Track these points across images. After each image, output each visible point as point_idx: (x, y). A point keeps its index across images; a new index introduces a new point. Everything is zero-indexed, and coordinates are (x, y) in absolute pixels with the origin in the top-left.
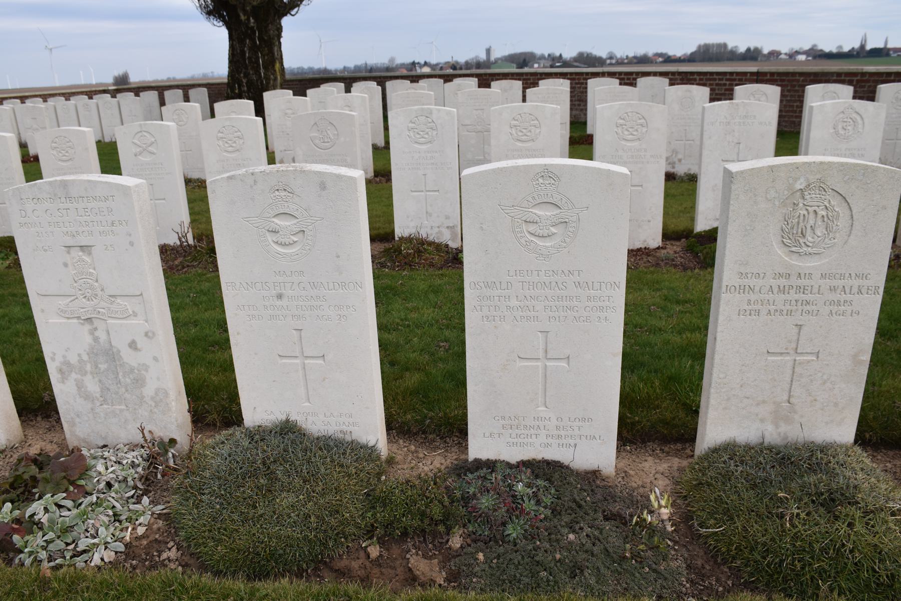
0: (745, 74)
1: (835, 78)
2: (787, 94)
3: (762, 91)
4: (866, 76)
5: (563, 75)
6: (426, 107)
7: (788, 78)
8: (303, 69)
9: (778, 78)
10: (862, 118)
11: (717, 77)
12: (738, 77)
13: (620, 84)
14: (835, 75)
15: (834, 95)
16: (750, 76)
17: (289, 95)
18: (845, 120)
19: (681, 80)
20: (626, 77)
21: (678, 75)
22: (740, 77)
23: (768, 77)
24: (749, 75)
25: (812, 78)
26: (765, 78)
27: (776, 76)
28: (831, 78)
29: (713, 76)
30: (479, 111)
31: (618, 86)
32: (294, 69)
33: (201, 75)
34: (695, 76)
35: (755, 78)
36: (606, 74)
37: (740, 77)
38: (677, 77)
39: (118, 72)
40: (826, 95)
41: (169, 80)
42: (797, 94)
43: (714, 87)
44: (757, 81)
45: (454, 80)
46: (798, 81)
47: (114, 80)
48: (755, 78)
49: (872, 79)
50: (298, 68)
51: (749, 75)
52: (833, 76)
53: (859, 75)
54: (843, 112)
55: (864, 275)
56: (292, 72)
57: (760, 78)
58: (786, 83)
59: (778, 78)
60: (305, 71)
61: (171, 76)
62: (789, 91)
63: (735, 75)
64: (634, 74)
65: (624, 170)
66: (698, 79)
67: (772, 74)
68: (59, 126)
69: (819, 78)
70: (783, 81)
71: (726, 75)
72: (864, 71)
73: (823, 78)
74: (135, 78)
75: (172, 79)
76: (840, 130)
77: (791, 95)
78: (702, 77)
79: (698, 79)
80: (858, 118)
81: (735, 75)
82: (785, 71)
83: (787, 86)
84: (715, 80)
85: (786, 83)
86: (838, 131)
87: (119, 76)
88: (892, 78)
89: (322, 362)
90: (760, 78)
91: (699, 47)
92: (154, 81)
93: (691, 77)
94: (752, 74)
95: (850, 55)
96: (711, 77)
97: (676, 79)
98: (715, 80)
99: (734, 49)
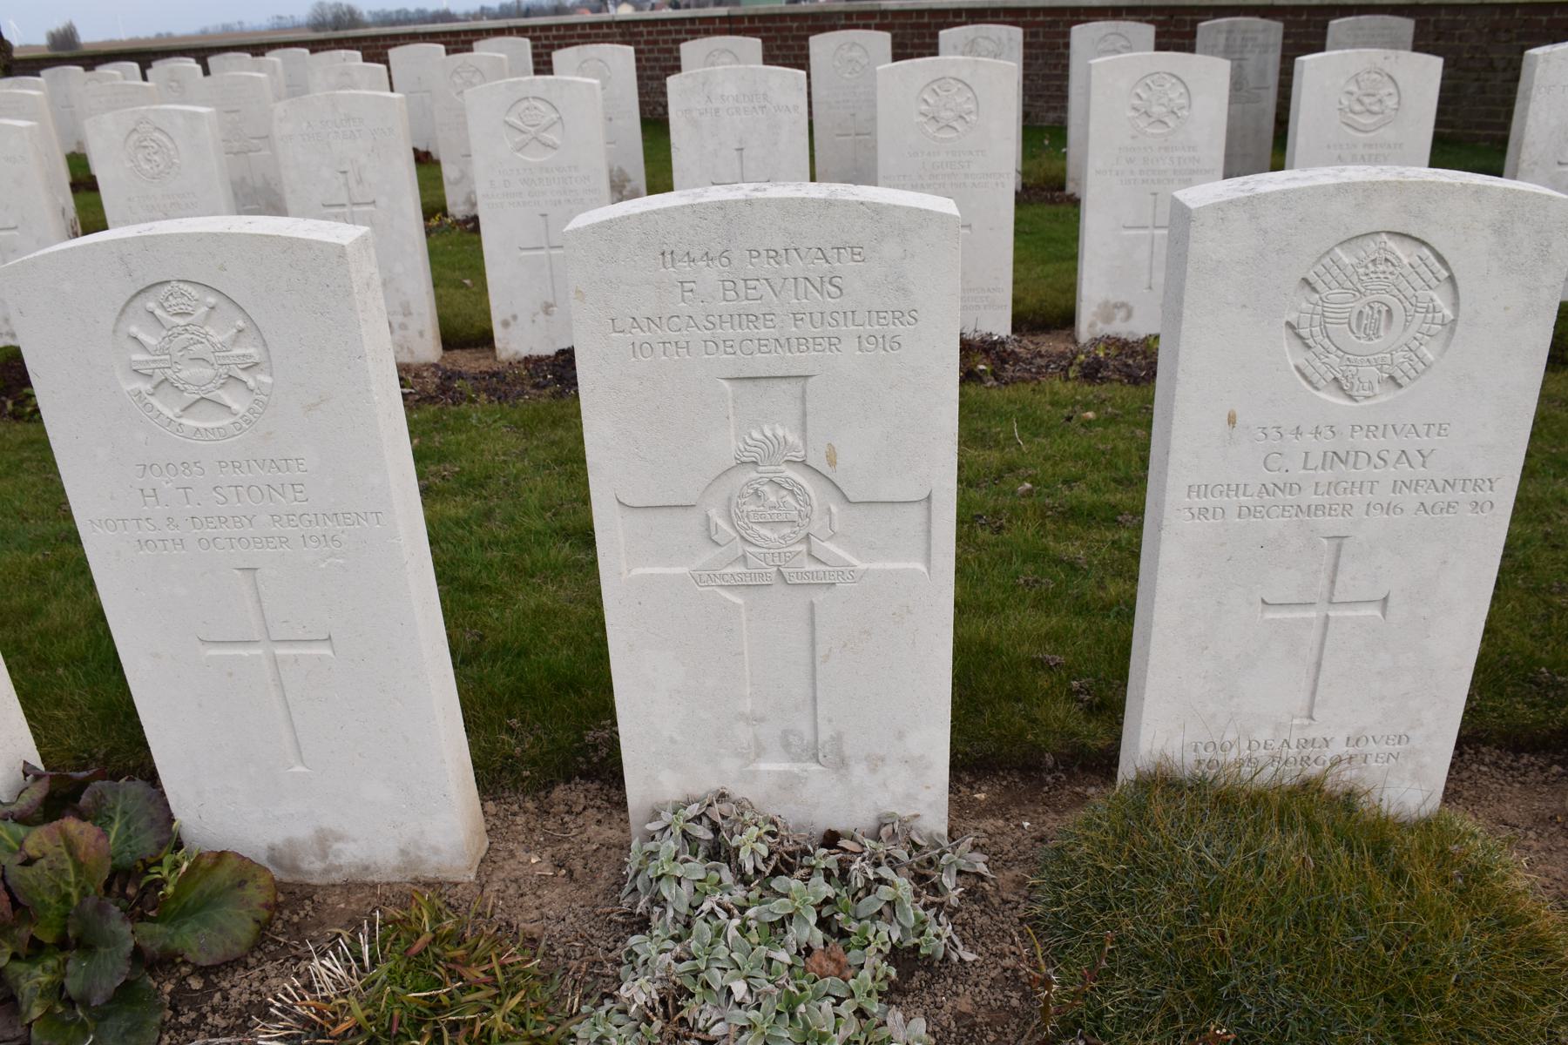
0: (711, 19)
1: (843, 22)
2: (777, 53)
3: (471, 66)
4: (887, 18)
5: (521, 31)
6: (346, 92)
7: (774, 25)
8: (407, 13)
9: (761, 25)
10: (171, 139)
11: (672, 28)
12: (702, 27)
13: (448, 52)
14: (843, 17)
15: (600, 64)
16: (720, 23)
17: (356, 60)
18: (145, 143)
19: (622, 35)
20: (542, 34)
21: (616, 27)
22: (706, 26)
23: (746, 24)
24: (717, 21)
25: (810, 23)
26: (742, 26)
27: (756, 21)
28: (837, 23)
29: (666, 25)
30: (233, 115)
31: (361, 63)
32: (390, 13)
33: (220, 27)
34: (641, 28)
35: (727, 26)
36: (515, 31)
37: (706, 26)
38: (615, 30)
39: (57, 24)
40: (585, 65)
41: (227, 29)
42: (792, 53)
43: (642, 46)
44: (731, 32)
45: (267, 54)
46: (790, 29)
47: (48, 38)
48: (727, 26)
49: (897, 21)
50: (398, 12)
51: (717, 21)
52: (840, 19)
53: (878, 16)
54: (135, 130)
55: (1210, 488)
56: (87, 44)
57: (734, 26)
58: (773, 34)
59: (761, 25)
60: (410, 16)
61: (164, 31)
62: (779, 48)
63: (697, 22)
64: (579, 28)
65: (948, 206)
66: (645, 33)
67: (752, 18)
68: (392, 90)
69: (820, 23)
70: (768, 30)
71: (685, 25)
72: (883, 8)
73: (826, 23)
74: (90, 35)
75: (394, 17)
76: (142, 163)
77: (784, 55)
78: (650, 29)
79: (645, 33)
80: (164, 139)
81: (697, 22)
82: (769, 12)
83: (775, 39)
84: (669, 32)
85: (773, 34)
86: (140, 166)
87: (58, 31)
88: (951, 19)
89: (329, 652)
90: (734, 26)
91: (223, 26)
92: (131, 41)
93: (636, 30)
94: (722, 19)
95: (475, 17)
96: (664, 28)
97: (613, 35)
98: (669, 32)
99: (321, 19)
